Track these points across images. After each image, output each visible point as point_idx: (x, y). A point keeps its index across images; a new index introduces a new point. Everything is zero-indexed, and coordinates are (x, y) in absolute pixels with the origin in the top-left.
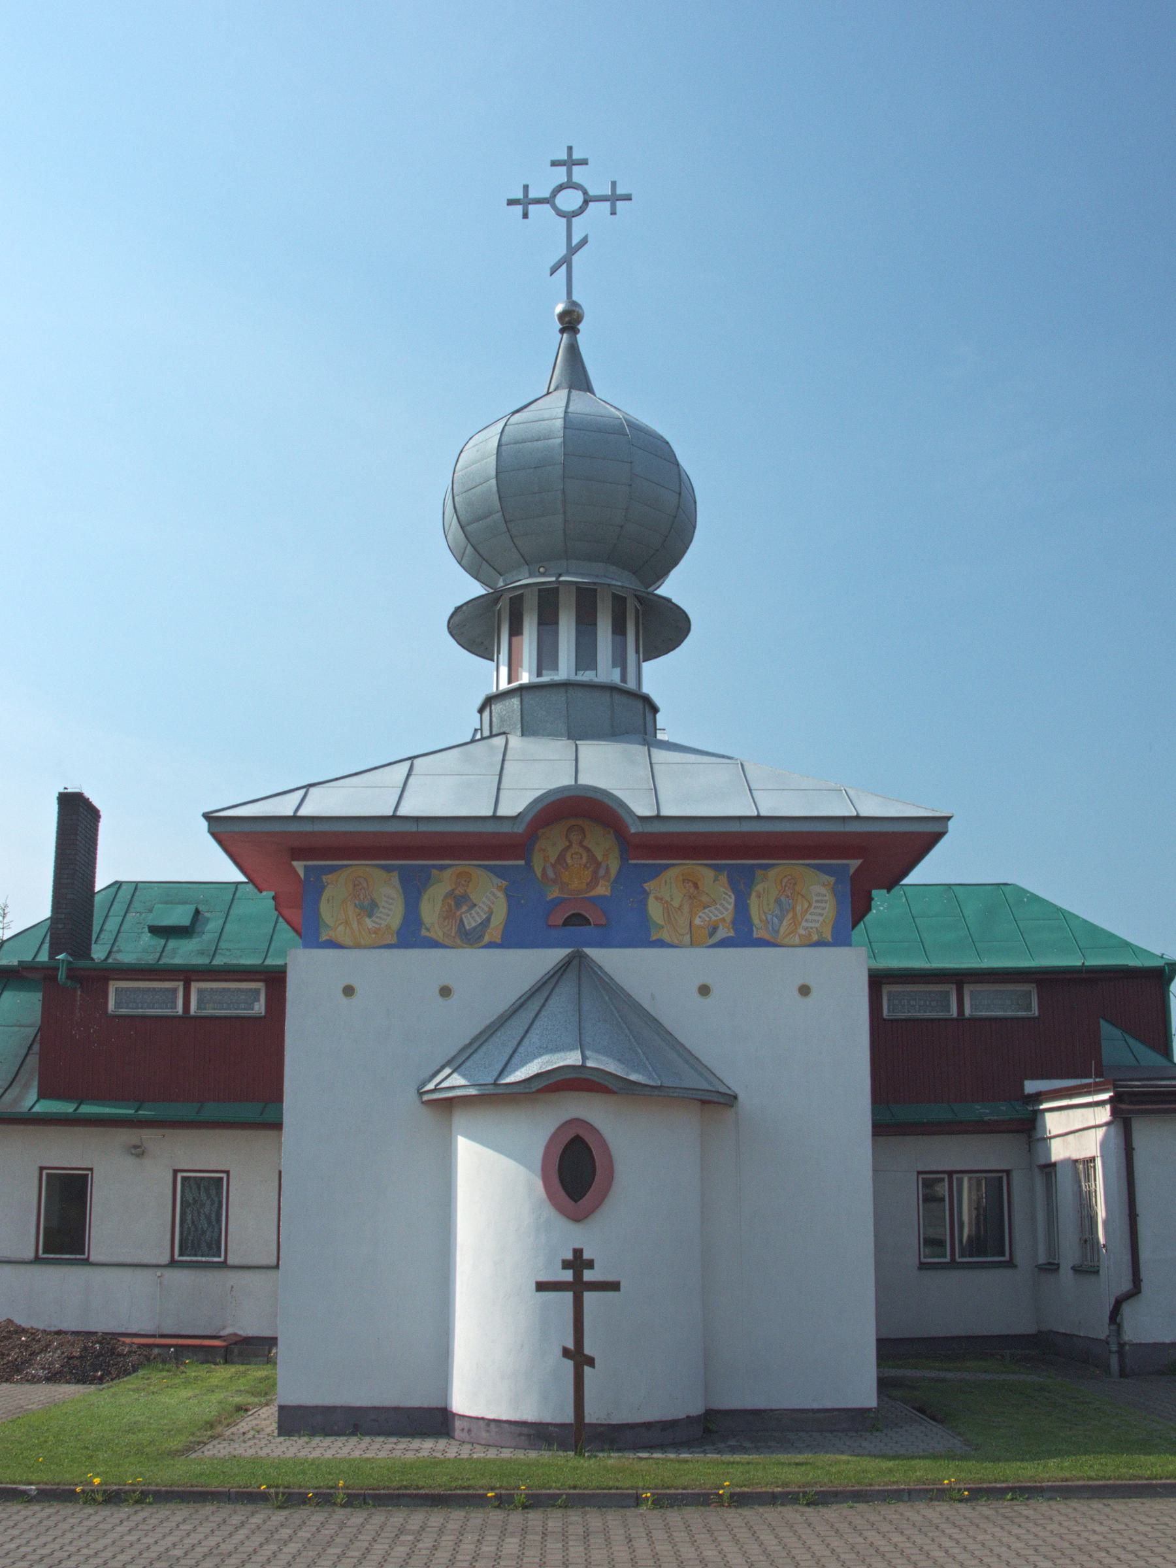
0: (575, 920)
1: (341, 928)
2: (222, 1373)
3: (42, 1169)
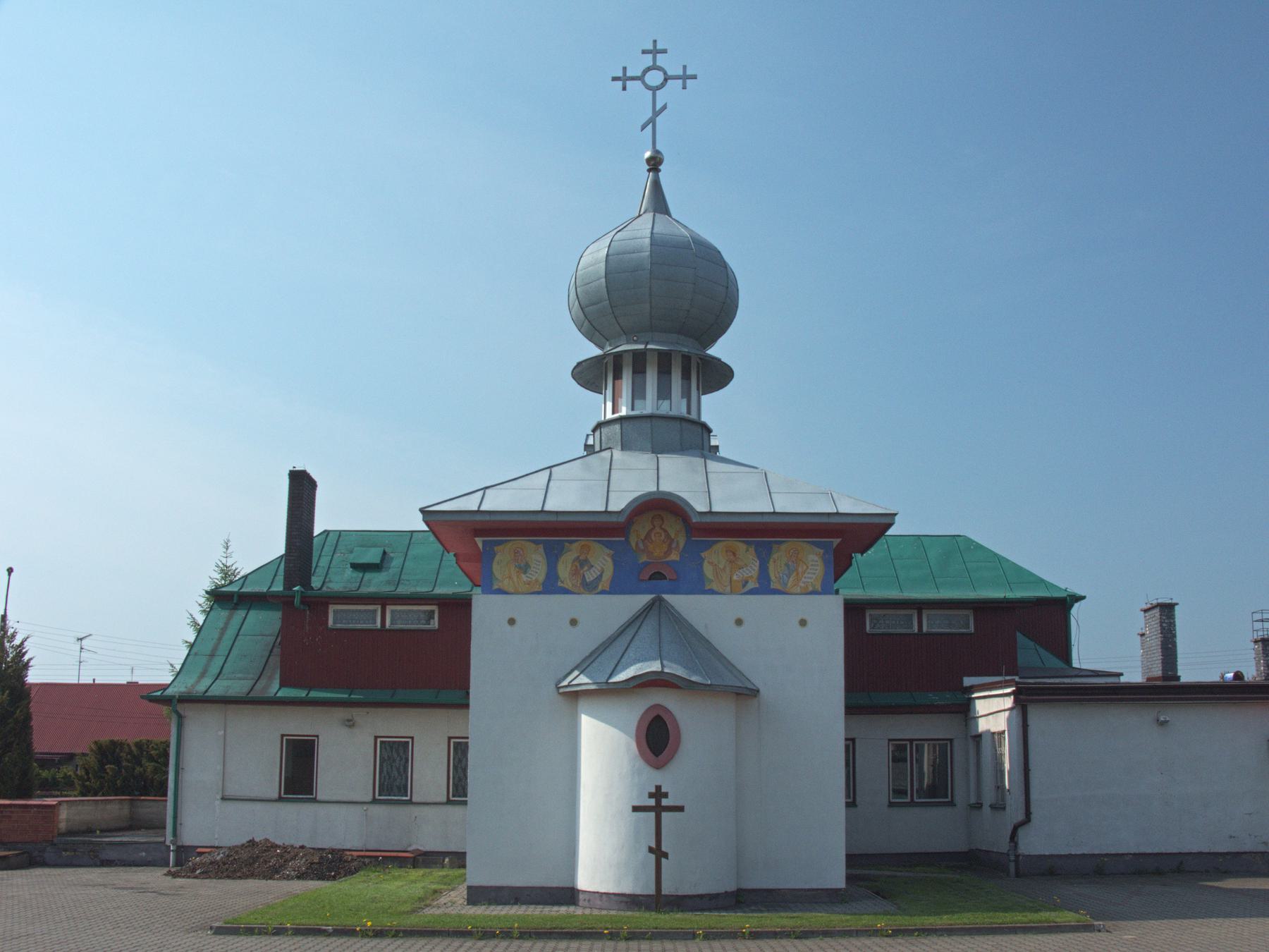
0: (658, 576)
1: (506, 582)
2: (415, 874)
3: (283, 736)
